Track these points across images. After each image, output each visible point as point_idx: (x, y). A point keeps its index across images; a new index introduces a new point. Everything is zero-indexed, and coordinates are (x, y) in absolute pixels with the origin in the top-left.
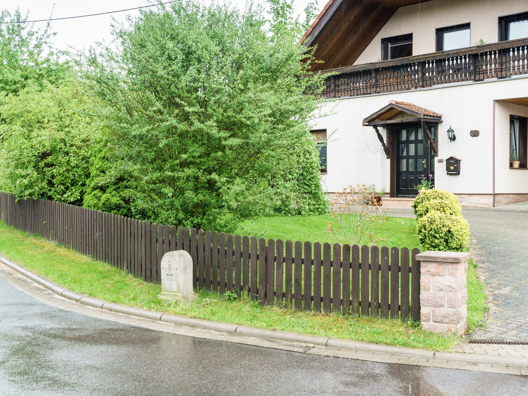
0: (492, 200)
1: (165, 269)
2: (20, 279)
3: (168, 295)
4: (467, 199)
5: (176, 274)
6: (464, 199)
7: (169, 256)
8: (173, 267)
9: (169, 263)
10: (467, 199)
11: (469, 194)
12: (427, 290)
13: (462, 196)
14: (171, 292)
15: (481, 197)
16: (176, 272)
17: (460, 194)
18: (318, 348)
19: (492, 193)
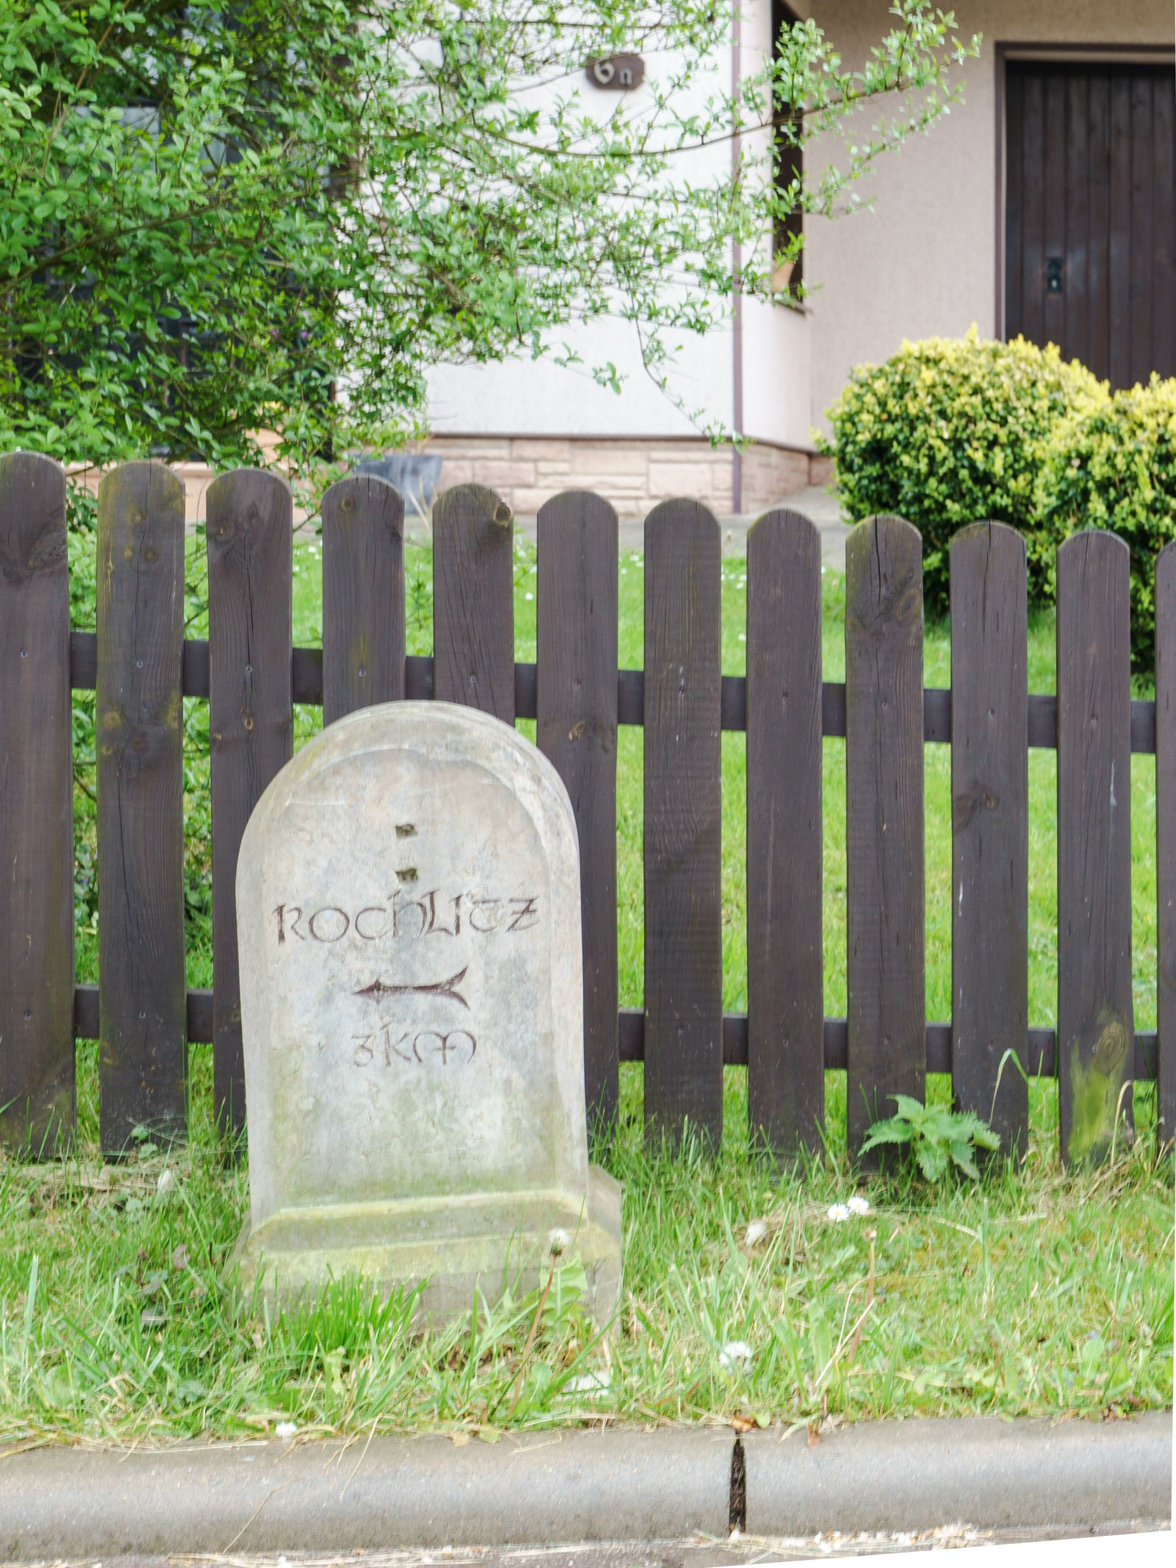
0: (724, 474)
1: (329, 924)
2: (553, 1085)
3: (395, 1227)
4: (562, 467)
5: (517, 963)
6: (544, 467)
7: (406, 773)
8: (472, 885)
9: (403, 852)
10: (562, 467)
11: (573, 439)
12: (1150, 990)
13: (528, 449)
14: (441, 1186)
15: (655, 455)
16: (507, 944)
17: (512, 438)
18: (400, 1560)
19: (719, 420)
